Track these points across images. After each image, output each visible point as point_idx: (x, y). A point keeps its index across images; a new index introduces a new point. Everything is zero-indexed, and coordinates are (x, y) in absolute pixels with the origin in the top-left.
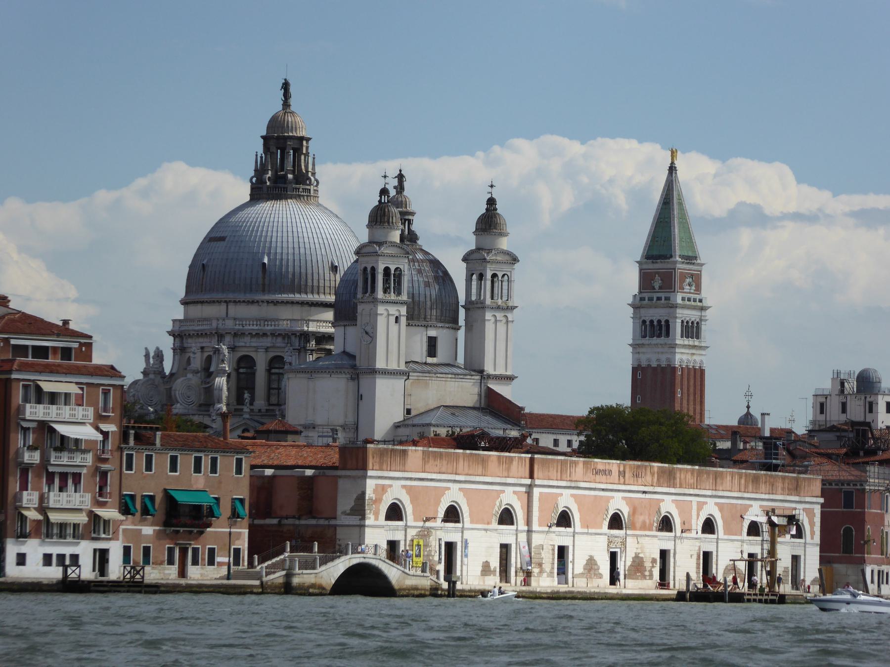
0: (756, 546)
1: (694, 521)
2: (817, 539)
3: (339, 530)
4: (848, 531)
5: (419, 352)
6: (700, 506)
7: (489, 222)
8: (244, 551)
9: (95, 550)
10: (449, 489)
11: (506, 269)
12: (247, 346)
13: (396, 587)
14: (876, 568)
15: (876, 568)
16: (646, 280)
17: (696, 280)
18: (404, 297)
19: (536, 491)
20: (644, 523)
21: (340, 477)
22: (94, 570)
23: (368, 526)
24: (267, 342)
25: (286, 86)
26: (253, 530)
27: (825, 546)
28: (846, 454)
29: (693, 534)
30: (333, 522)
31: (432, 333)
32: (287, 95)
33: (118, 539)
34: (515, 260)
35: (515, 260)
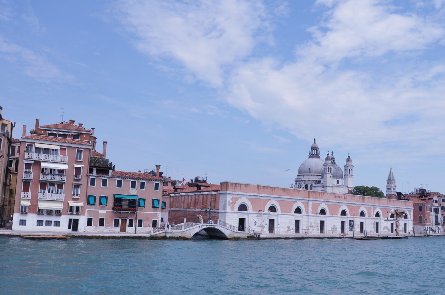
0: (392, 220)
1: (372, 213)
2: (412, 219)
3: (220, 214)
4: (421, 217)
5: (335, 183)
6: (374, 209)
7: (348, 160)
8: (158, 221)
9: (70, 220)
10: (271, 200)
11: (352, 168)
12: (307, 183)
13: (229, 237)
14: (429, 227)
15: (429, 227)
16: (388, 183)
17: (395, 183)
18: (332, 173)
19: (310, 203)
20: (354, 214)
21: (220, 194)
22: (69, 227)
23: (228, 213)
24: (310, 182)
25: (315, 139)
26: (170, 212)
27: (414, 220)
28: (419, 197)
29: (372, 217)
30: (218, 211)
31: (338, 180)
32: (315, 141)
33: (84, 215)
34: (353, 167)
35: (353, 167)
